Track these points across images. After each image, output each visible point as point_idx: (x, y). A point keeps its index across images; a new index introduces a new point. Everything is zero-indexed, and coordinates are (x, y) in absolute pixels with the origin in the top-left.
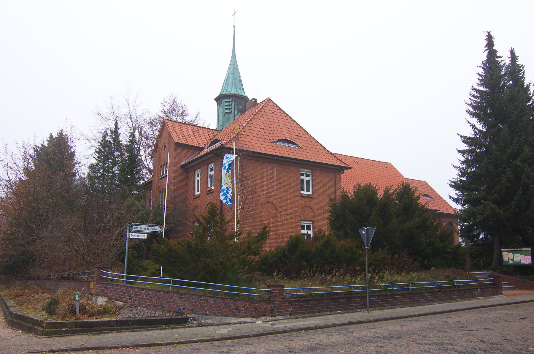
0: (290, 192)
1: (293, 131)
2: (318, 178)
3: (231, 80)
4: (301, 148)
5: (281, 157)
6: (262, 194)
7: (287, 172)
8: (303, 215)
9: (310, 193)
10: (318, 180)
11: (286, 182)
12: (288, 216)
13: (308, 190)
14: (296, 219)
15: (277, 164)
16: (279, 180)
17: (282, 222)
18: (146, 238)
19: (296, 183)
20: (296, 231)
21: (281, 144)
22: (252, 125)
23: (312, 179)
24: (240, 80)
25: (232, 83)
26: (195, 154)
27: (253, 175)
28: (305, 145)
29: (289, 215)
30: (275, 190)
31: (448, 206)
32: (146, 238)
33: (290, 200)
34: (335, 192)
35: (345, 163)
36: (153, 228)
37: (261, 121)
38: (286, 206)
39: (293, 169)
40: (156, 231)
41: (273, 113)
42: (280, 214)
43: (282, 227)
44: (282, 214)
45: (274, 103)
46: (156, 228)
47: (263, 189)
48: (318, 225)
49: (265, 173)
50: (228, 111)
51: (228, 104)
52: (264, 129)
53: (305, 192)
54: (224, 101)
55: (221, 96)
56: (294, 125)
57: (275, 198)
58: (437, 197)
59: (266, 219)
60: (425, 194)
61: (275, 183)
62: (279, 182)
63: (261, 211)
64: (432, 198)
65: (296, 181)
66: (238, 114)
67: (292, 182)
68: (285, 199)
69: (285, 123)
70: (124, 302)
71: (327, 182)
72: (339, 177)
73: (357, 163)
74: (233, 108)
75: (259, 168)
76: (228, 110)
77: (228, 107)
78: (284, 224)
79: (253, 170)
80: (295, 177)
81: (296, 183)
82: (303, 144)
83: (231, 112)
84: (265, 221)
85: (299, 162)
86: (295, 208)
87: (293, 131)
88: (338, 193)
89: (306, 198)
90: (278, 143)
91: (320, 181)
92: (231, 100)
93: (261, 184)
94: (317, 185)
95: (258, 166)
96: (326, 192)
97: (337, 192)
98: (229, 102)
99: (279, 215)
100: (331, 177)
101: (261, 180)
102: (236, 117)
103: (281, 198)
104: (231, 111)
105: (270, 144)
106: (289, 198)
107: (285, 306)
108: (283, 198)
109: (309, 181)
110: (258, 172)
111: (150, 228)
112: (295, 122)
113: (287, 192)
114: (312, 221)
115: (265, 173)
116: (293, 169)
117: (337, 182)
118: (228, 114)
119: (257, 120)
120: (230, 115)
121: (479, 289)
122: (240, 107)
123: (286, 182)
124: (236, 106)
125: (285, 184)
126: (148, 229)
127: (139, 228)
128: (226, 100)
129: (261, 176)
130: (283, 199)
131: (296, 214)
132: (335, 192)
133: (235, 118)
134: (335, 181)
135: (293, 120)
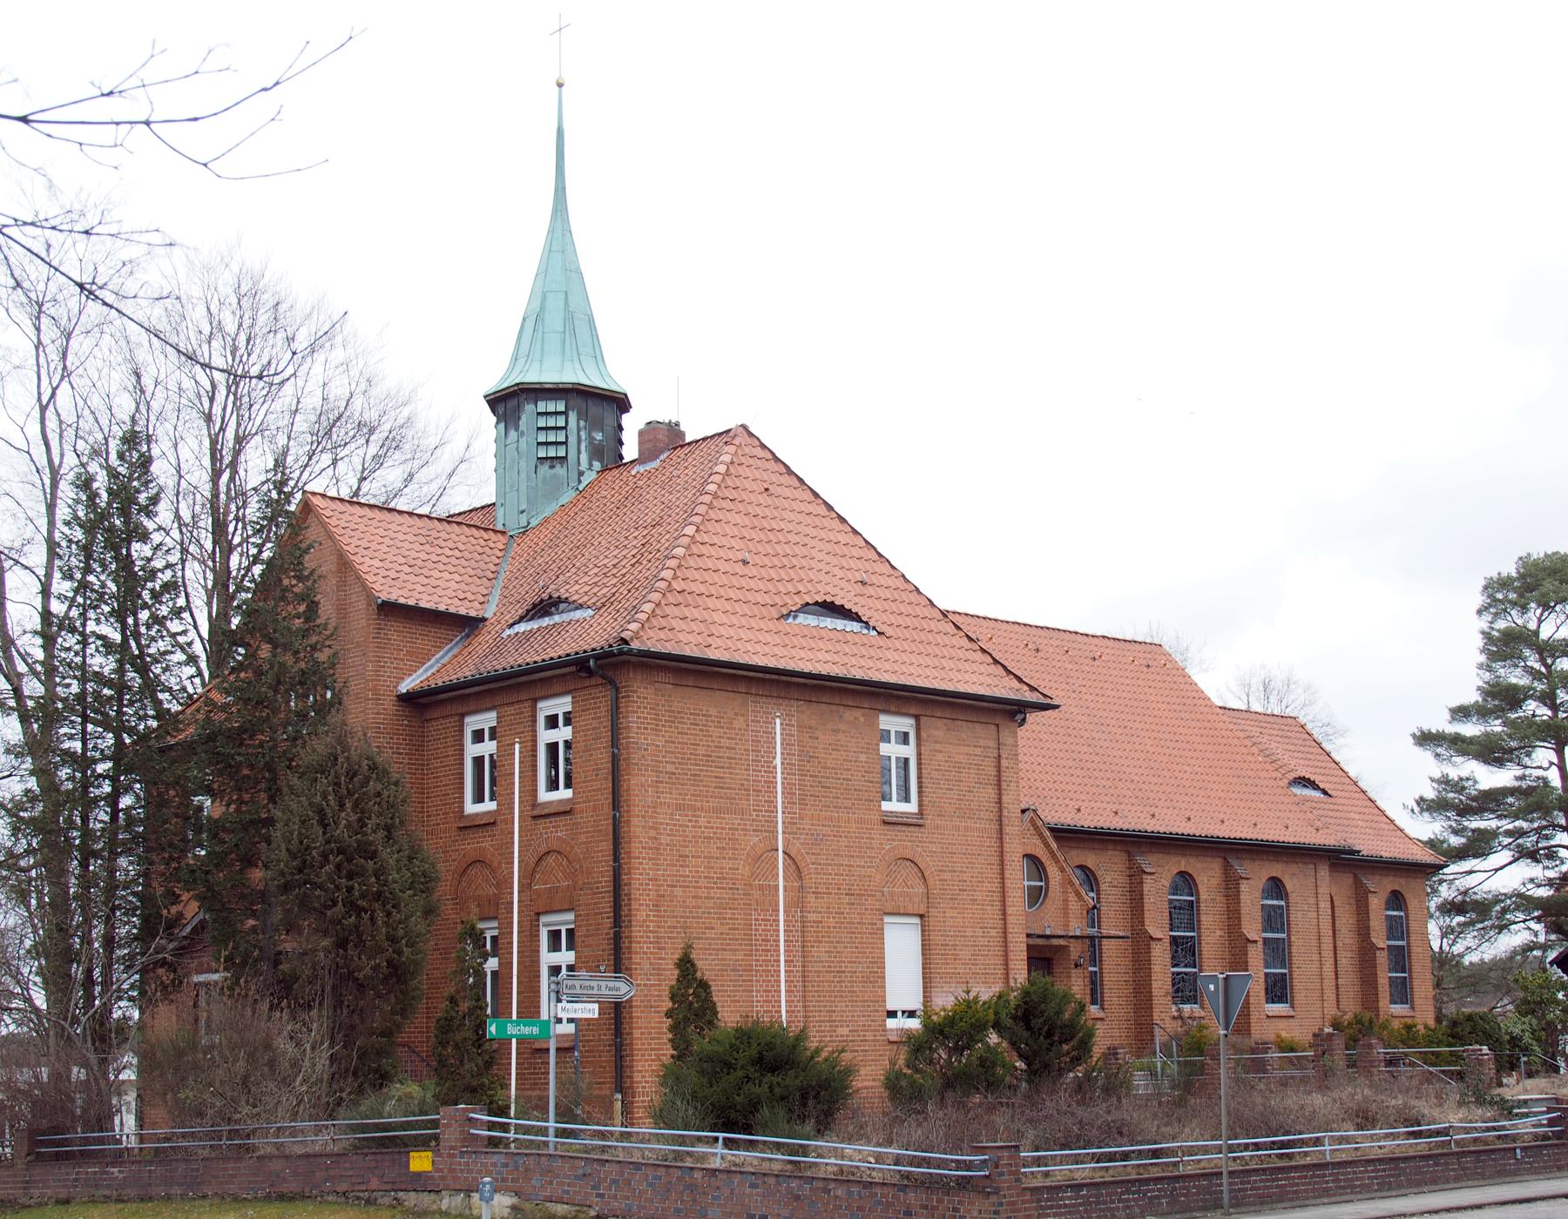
0: (845, 808)
1: (843, 562)
2: (938, 747)
3: (554, 320)
4: (879, 633)
5: (810, 676)
6: (753, 820)
7: (836, 731)
8: (892, 894)
9: (912, 807)
10: (940, 757)
11: (833, 768)
12: (839, 899)
13: (907, 799)
14: (866, 909)
15: (800, 703)
16: (808, 762)
17: (821, 922)
18: (596, 1016)
19: (866, 772)
20: (868, 957)
21: (812, 620)
22: (704, 550)
23: (919, 755)
24: (591, 321)
25: (564, 332)
26: (447, 644)
27: (721, 747)
28: (893, 619)
29: (842, 894)
30: (795, 803)
31: (1386, 827)
32: (596, 1016)
33: (846, 837)
34: (1000, 799)
35: (1032, 689)
36: (611, 984)
37: (730, 530)
38: (833, 860)
39: (855, 718)
40: (618, 993)
41: (767, 490)
42: (813, 893)
43: (821, 942)
44: (820, 893)
45: (763, 446)
46: (618, 984)
47: (754, 800)
48: (939, 931)
49: (762, 737)
50: (552, 453)
51: (551, 422)
52: (745, 562)
53: (893, 806)
54: (529, 408)
55: (520, 389)
56: (856, 552)
57: (796, 833)
58: (1346, 787)
59: (765, 915)
60: (1300, 778)
61: (795, 774)
62: (809, 771)
63: (750, 884)
64: (1325, 792)
65: (866, 762)
66: (591, 465)
67: (850, 770)
68: (829, 836)
69: (813, 532)
70: (578, 1205)
71: (971, 764)
72: (1010, 741)
73: (1038, 650)
74: (573, 440)
75: (741, 719)
76: (549, 447)
77: (552, 438)
78: (826, 932)
79: (723, 728)
80: (863, 748)
81: (866, 772)
82: (885, 618)
83: (563, 459)
84: (762, 920)
85: (877, 690)
86: (864, 867)
87: (843, 562)
88: (1009, 804)
89: (900, 827)
90: (799, 620)
91: (946, 761)
92: (561, 408)
93: (747, 780)
94: (935, 774)
95: (736, 714)
96: (967, 800)
97: (1005, 799)
98: (557, 413)
99: (811, 898)
100: (982, 743)
101: (748, 765)
102: (586, 480)
103: (816, 830)
104: (562, 453)
105: (772, 625)
106: (844, 832)
107: (1024, 1202)
108: (821, 830)
109: (906, 760)
110: (737, 734)
111: (603, 984)
112: (846, 522)
113: (835, 807)
114: (921, 916)
115: (762, 737)
116: (855, 718)
117: (1004, 763)
118: (552, 467)
119: (718, 527)
120: (560, 470)
121: (1518, 1151)
122: (599, 436)
123: (833, 768)
124: (583, 434)
125: (827, 778)
126: (599, 988)
127: (578, 987)
128: (542, 406)
129: (748, 750)
130: (824, 835)
131: (866, 890)
132: (1000, 802)
133: (580, 482)
134: (999, 756)
135: (825, 503)
